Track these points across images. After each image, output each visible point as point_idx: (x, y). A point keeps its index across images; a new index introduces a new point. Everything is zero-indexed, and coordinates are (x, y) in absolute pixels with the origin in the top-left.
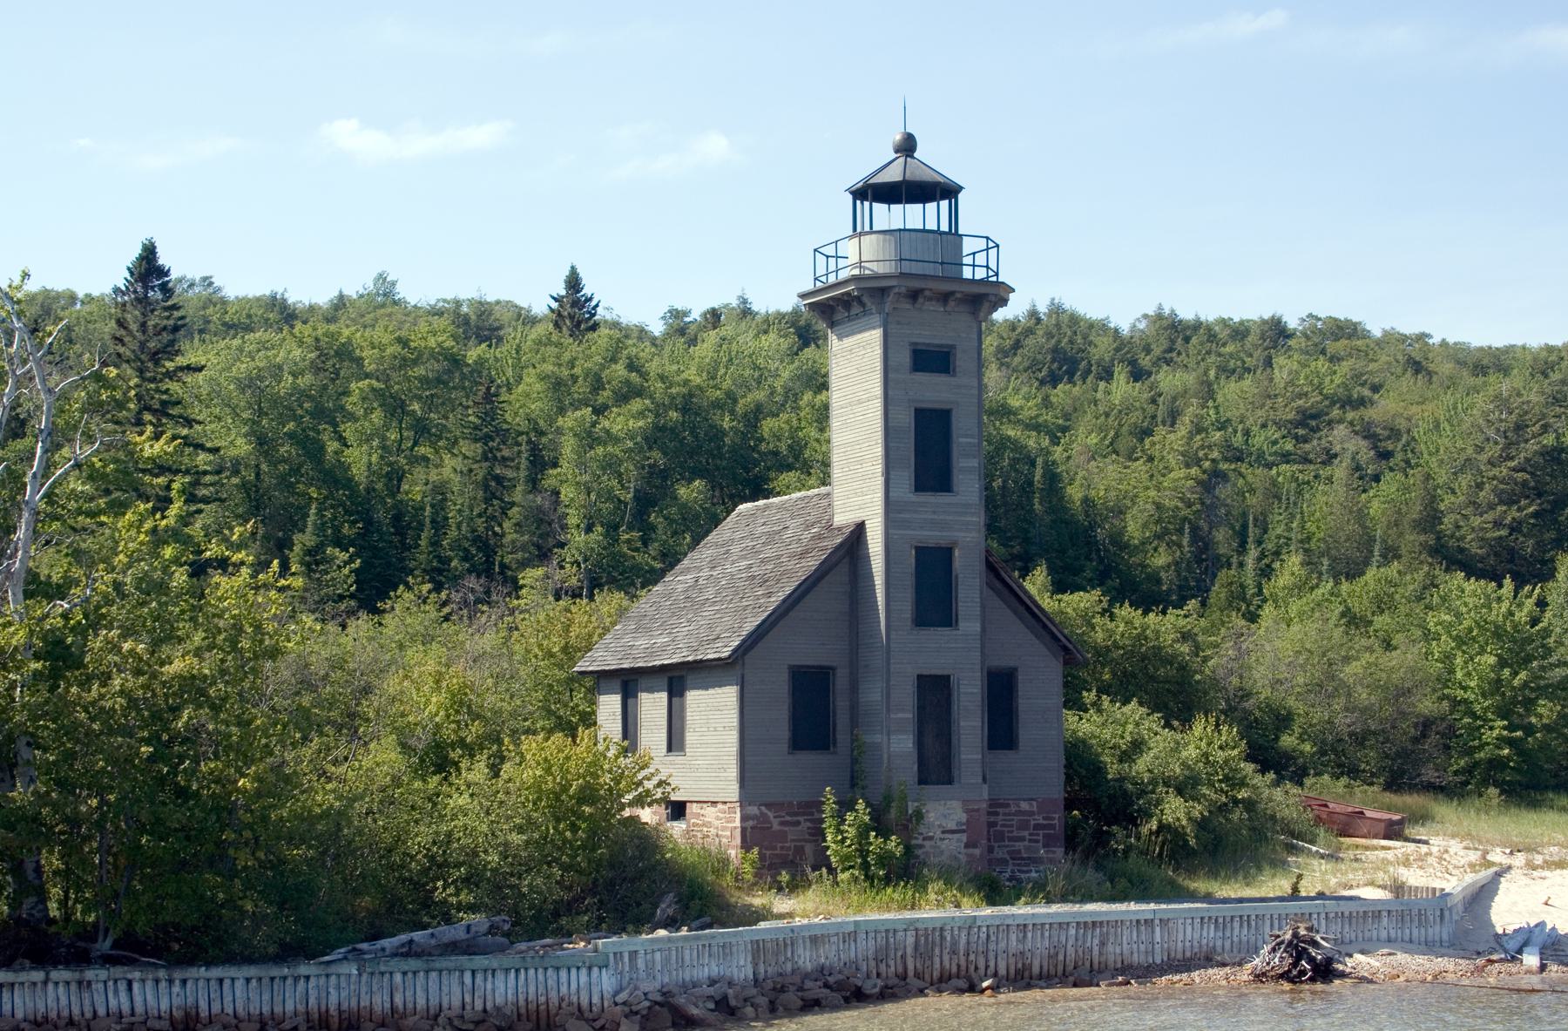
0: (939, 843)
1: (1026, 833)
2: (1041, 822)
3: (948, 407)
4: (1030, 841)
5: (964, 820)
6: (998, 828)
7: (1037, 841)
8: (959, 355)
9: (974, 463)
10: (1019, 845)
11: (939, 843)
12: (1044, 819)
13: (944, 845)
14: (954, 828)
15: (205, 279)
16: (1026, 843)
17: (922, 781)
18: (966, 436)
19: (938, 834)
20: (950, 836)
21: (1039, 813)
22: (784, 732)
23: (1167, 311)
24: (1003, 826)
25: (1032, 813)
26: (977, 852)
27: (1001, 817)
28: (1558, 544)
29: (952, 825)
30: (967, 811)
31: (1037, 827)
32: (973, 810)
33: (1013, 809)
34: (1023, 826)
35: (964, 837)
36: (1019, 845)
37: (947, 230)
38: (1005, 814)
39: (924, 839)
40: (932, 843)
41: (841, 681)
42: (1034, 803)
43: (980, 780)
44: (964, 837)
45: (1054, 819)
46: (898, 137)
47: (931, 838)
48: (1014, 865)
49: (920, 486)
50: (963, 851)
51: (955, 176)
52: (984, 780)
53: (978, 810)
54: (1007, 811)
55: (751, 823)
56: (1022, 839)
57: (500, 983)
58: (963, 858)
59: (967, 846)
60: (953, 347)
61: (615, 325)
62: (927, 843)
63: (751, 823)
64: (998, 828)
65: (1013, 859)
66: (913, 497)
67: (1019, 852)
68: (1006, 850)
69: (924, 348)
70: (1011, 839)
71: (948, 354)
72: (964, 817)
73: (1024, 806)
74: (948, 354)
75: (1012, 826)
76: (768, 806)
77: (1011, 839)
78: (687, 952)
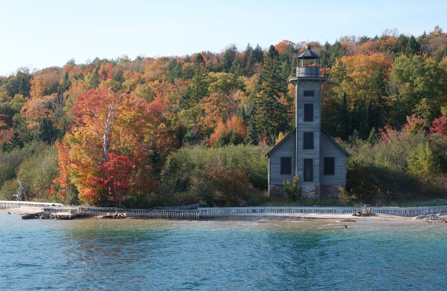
1: (336, 192)
9: (318, 115)
10: (334, 195)
13: (310, 194)
17: (305, 180)
19: (308, 191)
22: (279, 170)
23: (254, 48)
26: (318, 195)
28: (443, 102)
29: (311, 190)
30: (315, 187)
33: (333, 187)
35: (314, 192)
36: (334, 195)
41: (293, 160)
44: (314, 192)
47: (307, 192)
49: (305, 120)
56: (335, 193)
57: (180, 214)
58: (314, 197)
59: (315, 194)
60: (314, 91)
61: (38, 73)
62: (306, 193)
66: (304, 122)
70: (332, 193)
71: (313, 92)
74: (313, 92)
77: (332, 193)
78: (216, 211)
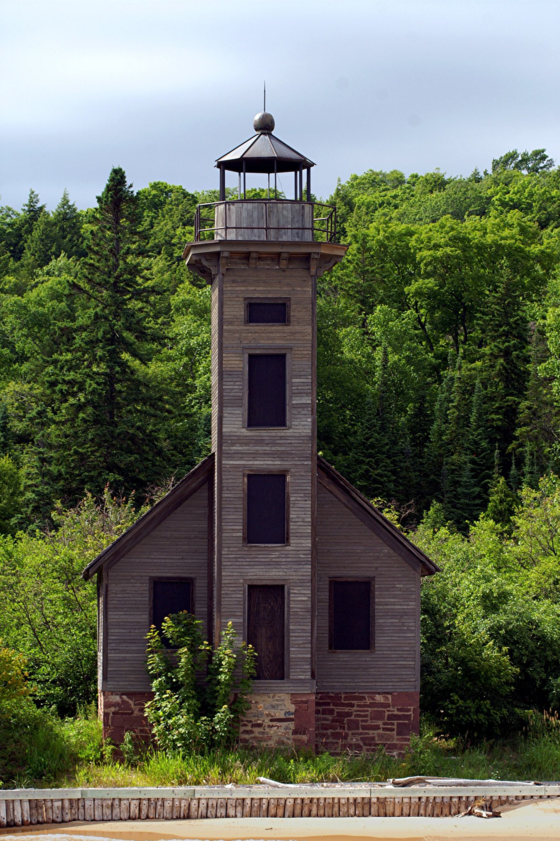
0: (267, 730)
1: (380, 723)
2: (396, 713)
3: (282, 352)
4: (384, 729)
5: (293, 710)
6: (353, 718)
7: (393, 730)
8: (293, 307)
11: (267, 730)
12: (398, 710)
13: (272, 731)
14: (282, 716)
15: (537, 153)
16: (380, 731)
18: (300, 377)
19: (267, 722)
20: (278, 724)
21: (394, 706)
24: (357, 716)
25: (387, 706)
26: (305, 738)
27: (355, 708)
29: (280, 715)
31: (391, 717)
32: (302, 702)
33: (368, 702)
34: (378, 716)
35: (292, 725)
37: (293, 198)
38: (358, 706)
39: (253, 726)
40: (261, 730)
42: (390, 697)
43: (310, 677)
44: (292, 725)
45: (409, 710)
46: (257, 117)
47: (260, 725)
48: (368, 750)
50: (292, 737)
51: (310, 157)
52: (313, 676)
53: (306, 702)
54: (362, 703)
55: (113, 709)
56: (377, 728)
59: (295, 732)
60: (289, 299)
62: (256, 730)
63: (113, 709)
64: (353, 718)
65: (365, 744)
67: (373, 739)
68: (359, 737)
69: (258, 301)
70: (364, 728)
72: (292, 708)
73: (379, 698)
74: (284, 305)
75: (366, 716)
76: (128, 694)
77: (364, 728)
